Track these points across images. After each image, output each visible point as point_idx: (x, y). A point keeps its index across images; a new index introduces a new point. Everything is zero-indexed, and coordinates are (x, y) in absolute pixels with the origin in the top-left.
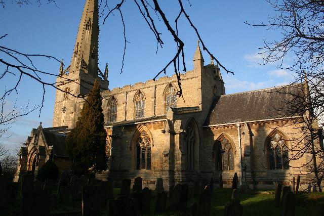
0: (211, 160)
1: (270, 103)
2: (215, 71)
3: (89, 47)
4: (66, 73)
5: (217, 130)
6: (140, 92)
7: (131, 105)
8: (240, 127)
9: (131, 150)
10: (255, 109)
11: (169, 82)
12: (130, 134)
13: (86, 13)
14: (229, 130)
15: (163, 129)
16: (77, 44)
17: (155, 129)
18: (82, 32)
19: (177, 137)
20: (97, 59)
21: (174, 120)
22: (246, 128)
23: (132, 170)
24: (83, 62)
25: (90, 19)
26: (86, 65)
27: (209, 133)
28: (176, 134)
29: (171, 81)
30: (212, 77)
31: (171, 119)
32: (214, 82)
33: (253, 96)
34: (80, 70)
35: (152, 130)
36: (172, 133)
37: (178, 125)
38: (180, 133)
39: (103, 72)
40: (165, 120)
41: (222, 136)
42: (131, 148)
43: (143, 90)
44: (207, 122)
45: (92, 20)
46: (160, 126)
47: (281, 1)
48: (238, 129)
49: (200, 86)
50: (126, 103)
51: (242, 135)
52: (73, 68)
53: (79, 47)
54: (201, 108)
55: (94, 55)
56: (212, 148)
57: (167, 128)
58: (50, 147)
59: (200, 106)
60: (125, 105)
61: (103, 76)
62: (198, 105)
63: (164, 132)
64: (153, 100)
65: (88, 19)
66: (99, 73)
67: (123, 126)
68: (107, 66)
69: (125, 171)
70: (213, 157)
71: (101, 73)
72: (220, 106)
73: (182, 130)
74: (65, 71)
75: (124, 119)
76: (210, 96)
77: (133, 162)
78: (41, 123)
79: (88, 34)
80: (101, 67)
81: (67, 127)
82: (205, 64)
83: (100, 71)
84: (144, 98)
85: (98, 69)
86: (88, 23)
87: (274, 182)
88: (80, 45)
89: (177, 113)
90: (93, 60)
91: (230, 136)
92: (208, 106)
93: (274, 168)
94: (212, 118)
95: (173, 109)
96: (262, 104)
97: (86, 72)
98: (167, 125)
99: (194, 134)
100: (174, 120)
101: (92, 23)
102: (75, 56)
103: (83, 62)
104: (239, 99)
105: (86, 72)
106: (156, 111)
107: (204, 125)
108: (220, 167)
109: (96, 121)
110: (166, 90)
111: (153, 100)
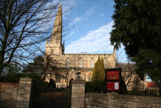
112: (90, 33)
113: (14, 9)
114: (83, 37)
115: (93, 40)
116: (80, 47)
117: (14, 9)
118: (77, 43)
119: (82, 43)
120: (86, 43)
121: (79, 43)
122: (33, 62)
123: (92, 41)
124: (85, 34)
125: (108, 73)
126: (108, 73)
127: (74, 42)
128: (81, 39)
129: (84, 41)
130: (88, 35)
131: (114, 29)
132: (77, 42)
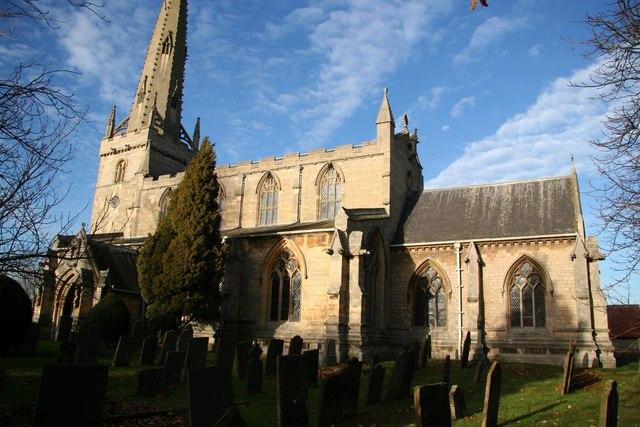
0: (406, 311)
1: (513, 209)
2: (410, 146)
3: (167, 85)
4: (120, 133)
5: (419, 252)
6: (269, 175)
7: (251, 200)
8: (461, 249)
9: (261, 284)
10: (486, 218)
11: (329, 159)
12: (258, 254)
13: (165, 22)
14: (437, 254)
15: (329, 247)
16: (143, 79)
17: (310, 245)
18: (155, 56)
19: (354, 266)
20: (180, 110)
21: (349, 231)
22: (472, 252)
23: (262, 322)
24: (155, 113)
25: (171, 33)
26: (160, 119)
27: (404, 256)
28: (352, 257)
29: (332, 158)
30: (405, 156)
31: (344, 228)
32: (408, 166)
33: (481, 195)
34: (151, 128)
35: (304, 248)
36: (347, 256)
37: (356, 239)
38: (360, 256)
39: (191, 133)
40: (332, 229)
41: (426, 264)
42: (261, 280)
43: (340, 163)
44: (399, 236)
45: (174, 36)
46: (320, 242)
47: (610, 10)
48: (458, 253)
49: (388, 170)
50: (243, 195)
51: (464, 264)
52: (135, 122)
53: (148, 84)
54: (388, 212)
55: (175, 102)
56: (406, 286)
57: (337, 245)
58: (104, 273)
59: (387, 208)
60: (239, 198)
61: (189, 141)
62: (384, 206)
63: (331, 252)
64: (297, 191)
65: (166, 34)
66: (183, 136)
67: (247, 238)
68: (198, 126)
69: (249, 322)
70: (408, 302)
71: (187, 136)
72: (421, 206)
73: (364, 251)
74: (119, 129)
75: (237, 225)
76: (402, 191)
77: (265, 305)
78: (84, 225)
79: (167, 60)
80: (189, 127)
81: (122, 234)
82: (397, 130)
83: (184, 132)
84: (277, 187)
85: (181, 127)
86: (167, 40)
87: (519, 350)
88: (149, 80)
89: (355, 218)
90: (173, 111)
91: (441, 264)
92: (399, 207)
93: (518, 324)
94: (407, 232)
95: (348, 211)
96: (498, 210)
97: (161, 132)
98: (337, 240)
99: (377, 259)
100: (349, 231)
101: (174, 41)
102: (139, 102)
103: (155, 113)
104: (455, 201)
105: (161, 132)
106: (302, 213)
107: (394, 242)
108: (421, 318)
109: (206, 229)
110: (260, 183)
111: (297, 191)
112: (551, 93)
113: (601, 331)
114: (518, 116)
115: (565, 125)
116: (500, 167)
117: (601, 331)
118: (489, 149)
119: (509, 146)
120: (531, 142)
121: (498, 147)
122: (361, 233)
123: (556, 128)
124: (523, 102)
125: (177, 350)
126: (177, 350)
127: (474, 145)
128: (503, 129)
129: (517, 136)
130: (539, 102)
131: (624, 103)
132: (487, 142)
